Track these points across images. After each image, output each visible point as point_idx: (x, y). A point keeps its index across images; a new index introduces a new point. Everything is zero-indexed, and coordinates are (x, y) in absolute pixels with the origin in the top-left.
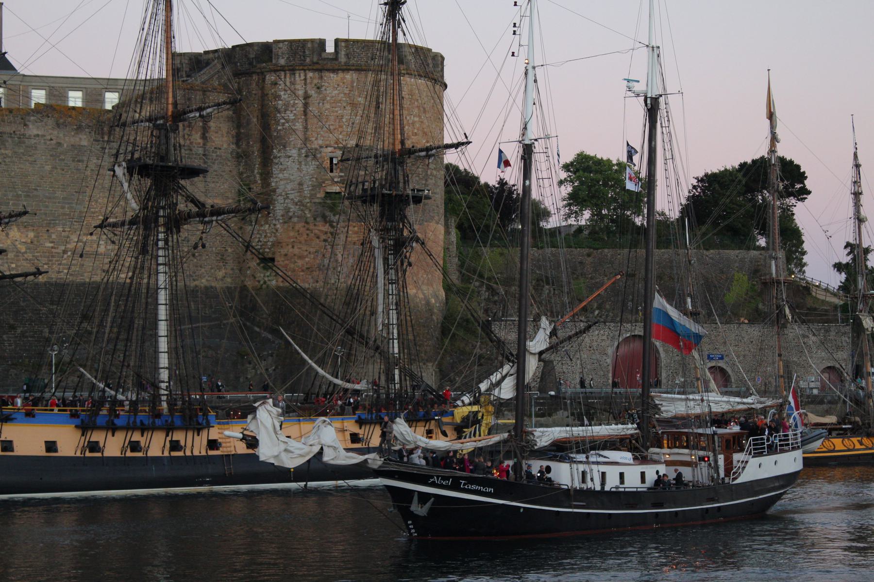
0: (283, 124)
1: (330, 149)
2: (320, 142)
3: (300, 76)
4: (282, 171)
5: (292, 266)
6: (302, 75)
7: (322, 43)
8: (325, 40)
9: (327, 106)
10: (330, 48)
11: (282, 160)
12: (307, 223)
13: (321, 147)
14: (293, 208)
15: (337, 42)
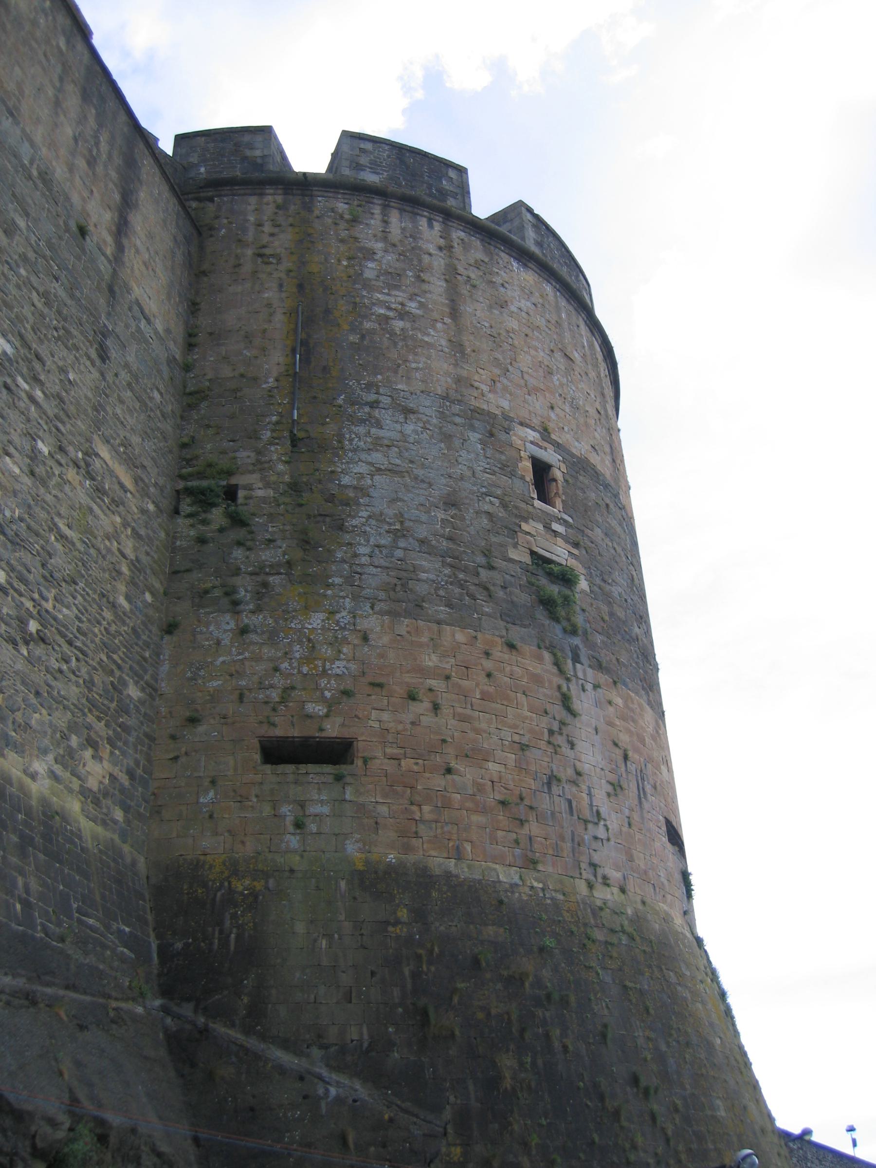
4: (377, 444)
5: (438, 782)
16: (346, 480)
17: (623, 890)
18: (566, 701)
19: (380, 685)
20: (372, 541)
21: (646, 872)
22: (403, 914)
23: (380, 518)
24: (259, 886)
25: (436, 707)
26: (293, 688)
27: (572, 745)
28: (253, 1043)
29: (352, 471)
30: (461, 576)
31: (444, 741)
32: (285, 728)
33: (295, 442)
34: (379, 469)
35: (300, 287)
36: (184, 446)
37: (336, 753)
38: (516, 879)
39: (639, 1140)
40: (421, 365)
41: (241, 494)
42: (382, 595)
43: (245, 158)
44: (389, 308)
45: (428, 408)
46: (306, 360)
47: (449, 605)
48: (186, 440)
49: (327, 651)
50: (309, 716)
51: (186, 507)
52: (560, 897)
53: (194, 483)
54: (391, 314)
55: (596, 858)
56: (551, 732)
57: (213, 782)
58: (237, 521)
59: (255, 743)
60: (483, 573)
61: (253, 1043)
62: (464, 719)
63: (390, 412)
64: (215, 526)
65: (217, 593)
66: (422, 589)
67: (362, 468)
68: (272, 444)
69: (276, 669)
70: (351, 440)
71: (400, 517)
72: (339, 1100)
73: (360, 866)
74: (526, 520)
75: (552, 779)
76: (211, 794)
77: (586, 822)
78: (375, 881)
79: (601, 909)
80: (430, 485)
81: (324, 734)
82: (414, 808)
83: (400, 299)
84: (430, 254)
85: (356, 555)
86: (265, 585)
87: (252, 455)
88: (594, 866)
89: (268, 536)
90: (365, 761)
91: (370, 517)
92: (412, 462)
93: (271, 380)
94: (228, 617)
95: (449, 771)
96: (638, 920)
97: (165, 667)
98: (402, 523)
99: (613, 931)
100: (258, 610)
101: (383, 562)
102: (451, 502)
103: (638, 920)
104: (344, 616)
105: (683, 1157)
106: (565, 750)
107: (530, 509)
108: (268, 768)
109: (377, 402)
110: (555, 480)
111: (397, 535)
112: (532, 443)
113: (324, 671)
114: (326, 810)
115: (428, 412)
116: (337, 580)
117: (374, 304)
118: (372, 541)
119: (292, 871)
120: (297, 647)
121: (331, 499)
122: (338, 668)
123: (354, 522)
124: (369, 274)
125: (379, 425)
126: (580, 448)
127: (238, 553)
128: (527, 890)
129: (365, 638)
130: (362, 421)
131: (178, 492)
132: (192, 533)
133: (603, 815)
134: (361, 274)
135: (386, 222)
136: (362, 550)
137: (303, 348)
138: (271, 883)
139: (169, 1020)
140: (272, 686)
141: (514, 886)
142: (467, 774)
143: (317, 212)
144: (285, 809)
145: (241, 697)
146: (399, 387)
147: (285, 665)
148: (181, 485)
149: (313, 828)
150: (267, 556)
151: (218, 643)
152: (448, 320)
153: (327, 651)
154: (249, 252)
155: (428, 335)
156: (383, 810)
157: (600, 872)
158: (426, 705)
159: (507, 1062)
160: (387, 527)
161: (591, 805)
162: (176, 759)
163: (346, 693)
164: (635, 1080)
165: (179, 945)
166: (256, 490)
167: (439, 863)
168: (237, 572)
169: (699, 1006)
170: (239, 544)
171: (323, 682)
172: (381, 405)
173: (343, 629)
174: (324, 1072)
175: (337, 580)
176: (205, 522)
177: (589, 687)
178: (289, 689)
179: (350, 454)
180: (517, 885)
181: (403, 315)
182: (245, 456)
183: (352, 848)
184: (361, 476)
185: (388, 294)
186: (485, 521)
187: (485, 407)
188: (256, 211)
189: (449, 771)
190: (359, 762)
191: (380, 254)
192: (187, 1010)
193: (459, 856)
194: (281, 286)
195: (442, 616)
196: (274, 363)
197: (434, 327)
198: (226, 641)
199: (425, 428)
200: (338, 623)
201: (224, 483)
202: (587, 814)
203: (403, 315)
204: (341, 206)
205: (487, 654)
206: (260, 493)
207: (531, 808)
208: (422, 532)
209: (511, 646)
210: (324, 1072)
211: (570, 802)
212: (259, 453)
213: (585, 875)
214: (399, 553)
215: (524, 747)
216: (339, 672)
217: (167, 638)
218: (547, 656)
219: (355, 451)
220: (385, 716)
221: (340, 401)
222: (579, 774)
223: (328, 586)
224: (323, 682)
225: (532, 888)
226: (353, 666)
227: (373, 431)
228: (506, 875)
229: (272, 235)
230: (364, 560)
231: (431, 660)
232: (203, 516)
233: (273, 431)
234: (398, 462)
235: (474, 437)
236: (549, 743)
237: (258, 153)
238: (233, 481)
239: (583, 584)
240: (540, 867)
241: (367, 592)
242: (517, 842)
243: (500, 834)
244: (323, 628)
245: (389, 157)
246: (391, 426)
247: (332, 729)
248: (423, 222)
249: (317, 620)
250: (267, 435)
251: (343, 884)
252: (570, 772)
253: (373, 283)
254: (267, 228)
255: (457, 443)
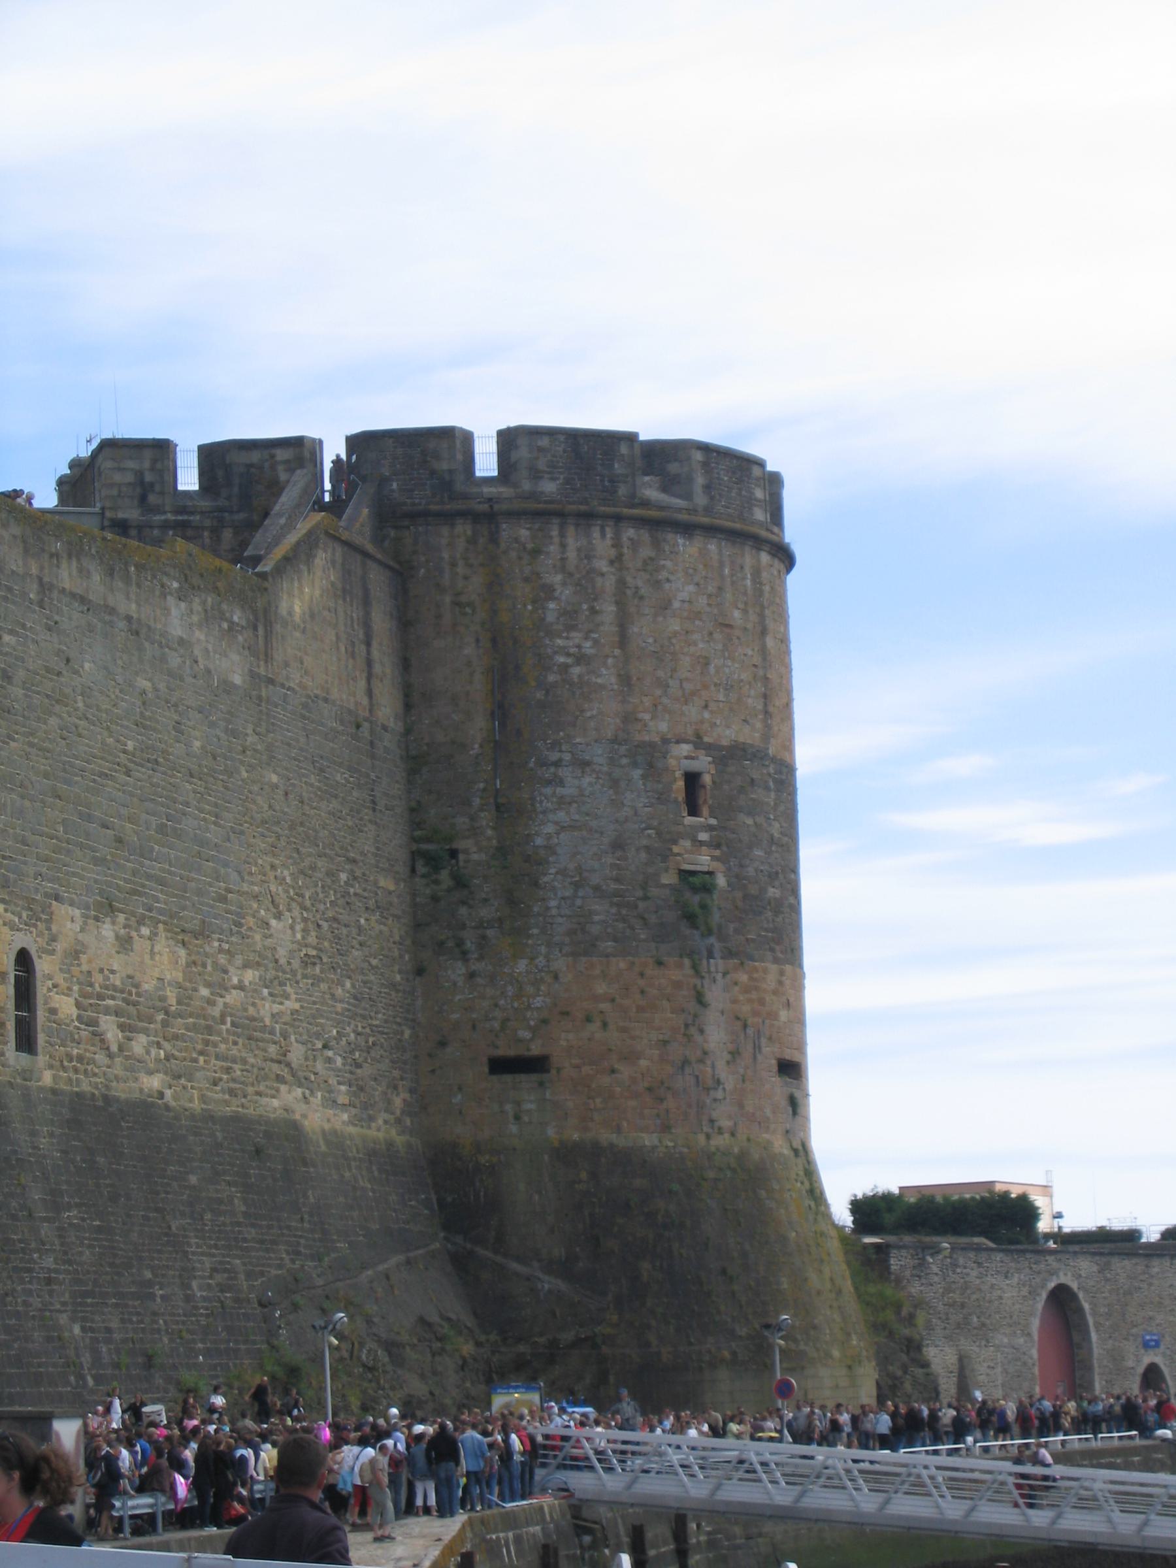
0: (565, 668)
1: (685, 749)
2: (663, 726)
3: (603, 535)
4: (563, 802)
5: (606, 1080)
6: (609, 533)
7: (162, 450)
8: (321, 442)
9: (675, 625)
10: (486, 463)
11: (561, 772)
12: (302, 802)
13: (665, 741)
14: (601, 910)
15: (508, 439)
16: (539, 841)
17: (733, 1134)
18: (700, 999)
19: (567, 1014)
20: (560, 894)
21: (753, 1114)
22: (584, 1175)
23: (563, 872)
24: (495, 1159)
25: (605, 1025)
26: (508, 1020)
27: (702, 1031)
28: (499, 1259)
29: (544, 831)
30: (624, 912)
31: (610, 1050)
32: (506, 1050)
33: (498, 807)
34: (563, 827)
35: (494, 641)
36: (412, 810)
37: (534, 1065)
38: (656, 1142)
39: (723, 1308)
40: (594, 712)
41: (461, 857)
42: (567, 940)
43: (433, 473)
44: (568, 655)
45: (598, 755)
46: (503, 725)
47: (615, 940)
48: (413, 804)
49: (530, 990)
50: (521, 1041)
51: (421, 869)
52: (686, 1150)
53: (425, 847)
54: (570, 661)
55: (714, 1115)
56: (687, 1026)
57: (460, 1089)
58: (460, 882)
59: (485, 1060)
60: (641, 905)
61: (499, 1259)
62: (624, 1030)
63: (570, 769)
64: (444, 886)
65: (450, 944)
66: (595, 930)
67: (550, 829)
68: (482, 810)
69: (496, 1005)
70: (541, 802)
71: (579, 869)
72: (550, 1291)
73: (556, 1144)
74: (675, 842)
75: (686, 1062)
76: (459, 1097)
77: (708, 1089)
78: (566, 1154)
79: (714, 1154)
80: (602, 833)
81: (531, 1053)
82: (591, 1101)
83: (577, 641)
84: (603, 575)
85: (548, 908)
86: (484, 937)
87: (467, 820)
88: (712, 1121)
89: (484, 896)
90: (559, 1070)
91: (557, 873)
92: (587, 814)
93: (476, 746)
94: (460, 964)
95: (613, 1071)
96: (743, 1156)
97: (419, 1002)
98: (580, 874)
99: (720, 1169)
100: (481, 958)
101: (567, 912)
102: (618, 845)
103: (743, 1156)
104: (540, 961)
105: (750, 1317)
106: (699, 1038)
107: (681, 829)
108: (494, 1078)
109: (561, 760)
110: (704, 787)
111: (577, 886)
112: (686, 758)
113: (529, 1005)
114: (533, 1106)
115: (600, 760)
116: (535, 931)
117: (556, 653)
118: (560, 894)
119: (514, 1149)
120: (510, 988)
121: (527, 859)
122: (538, 1002)
123: (546, 879)
124: (551, 618)
125: (561, 783)
126: (728, 733)
127: (463, 911)
128: (663, 1149)
129: (556, 977)
130: (549, 782)
131: (413, 853)
132: (428, 891)
133: (722, 1080)
134: (543, 619)
135: (563, 546)
136: (553, 903)
137: (500, 712)
138: (502, 1157)
139: (449, 1246)
140: (494, 1018)
141: (654, 1148)
142: (625, 1071)
143: (503, 546)
144: (509, 1107)
145: (474, 1027)
146: (578, 740)
147: (502, 1002)
148: (414, 847)
149: (526, 1119)
150: (485, 913)
151: (455, 984)
152: (617, 652)
153: (530, 990)
154: (448, 599)
155: (600, 676)
156: (570, 1104)
157: (717, 1124)
158: (599, 1024)
159: (645, 1266)
160: (569, 880)
161: (713, 1076)
162: (433, 1071)
163: (545, 1021)
164: (724, 1272)
165: (449, 1199)
166: (474, 853)
167: (606, 1137)
168: (463, 927)
169: (782, 1211)
170: (464, 903)
171: (529, 1014)
172: (564, 763)
173: (540, 971)
174: (541, 1275)
175: (535, 931)
176: (436, 882)
177: (719, 976)
178: (505, 1021)
179: (541, 816)
180: (657, 1147)
181: (581, 659)
182: (462, 821)
183: (551, 1132)
184: (549, 837)
185: (567, 638)
186: (643, 855)
187: (647, 738)
188: (451, 543)
189: (613, 1071)
190: (554, 1072)
191: (559, 589)
192: (459, 1239)
193: (618, 1130)
194: (477, 641)
195: (609, 950)
196: (478, 728)
197: (605, 664)
198: (460, 984)
199: (598, 778)
200: (537, 967)
201: (447, 847)
202: (710, 1083)
203: (581, 659)
204: (524, 533)
205: (642, 975)
206: (475, 857)
207: (669, 1088)
208: (595, 879)
209: (660, 963)
210: (541, 1275)
211: (697, 1077)
212: (472, 819)
213: (705, 1129)
214: (579, 902)
215: (665, 1043)
216: (538, 1005)
217: (418, 979)
218: (687, 962)
219: (544, 812)
220: (571, 1036)
221: (531, 765)
222: (705, 1053)
223: (529, 936)
224: (529, 1014)
225: (667, 1147)
226: (548, 1000)
227: (558, 790)
228: (648, 1140)
229: (466, 578)
230: (554, 912)
231: (601, 988)
232: (434, 876)
233: (481, 798)
234: (577, 817)
235: (637, 773)
236: (684, 1035)
237: (445, 466)
238: (455, 846)
239: (721, 881)
240: (673, 1131)
241: (557, 939)
242: (658, 1115)
243: (646, 1111)
244: (527, 972)
245: (564, 451)
246: (573, 783)
247: (536, 1050)
248: (596, 532)
249: (522, 965)
250: (477, 801)
251: (546, 1157)
252: (699, 1053)
253: (555, 627)
254: (461, 570)
255: (623, 784)
